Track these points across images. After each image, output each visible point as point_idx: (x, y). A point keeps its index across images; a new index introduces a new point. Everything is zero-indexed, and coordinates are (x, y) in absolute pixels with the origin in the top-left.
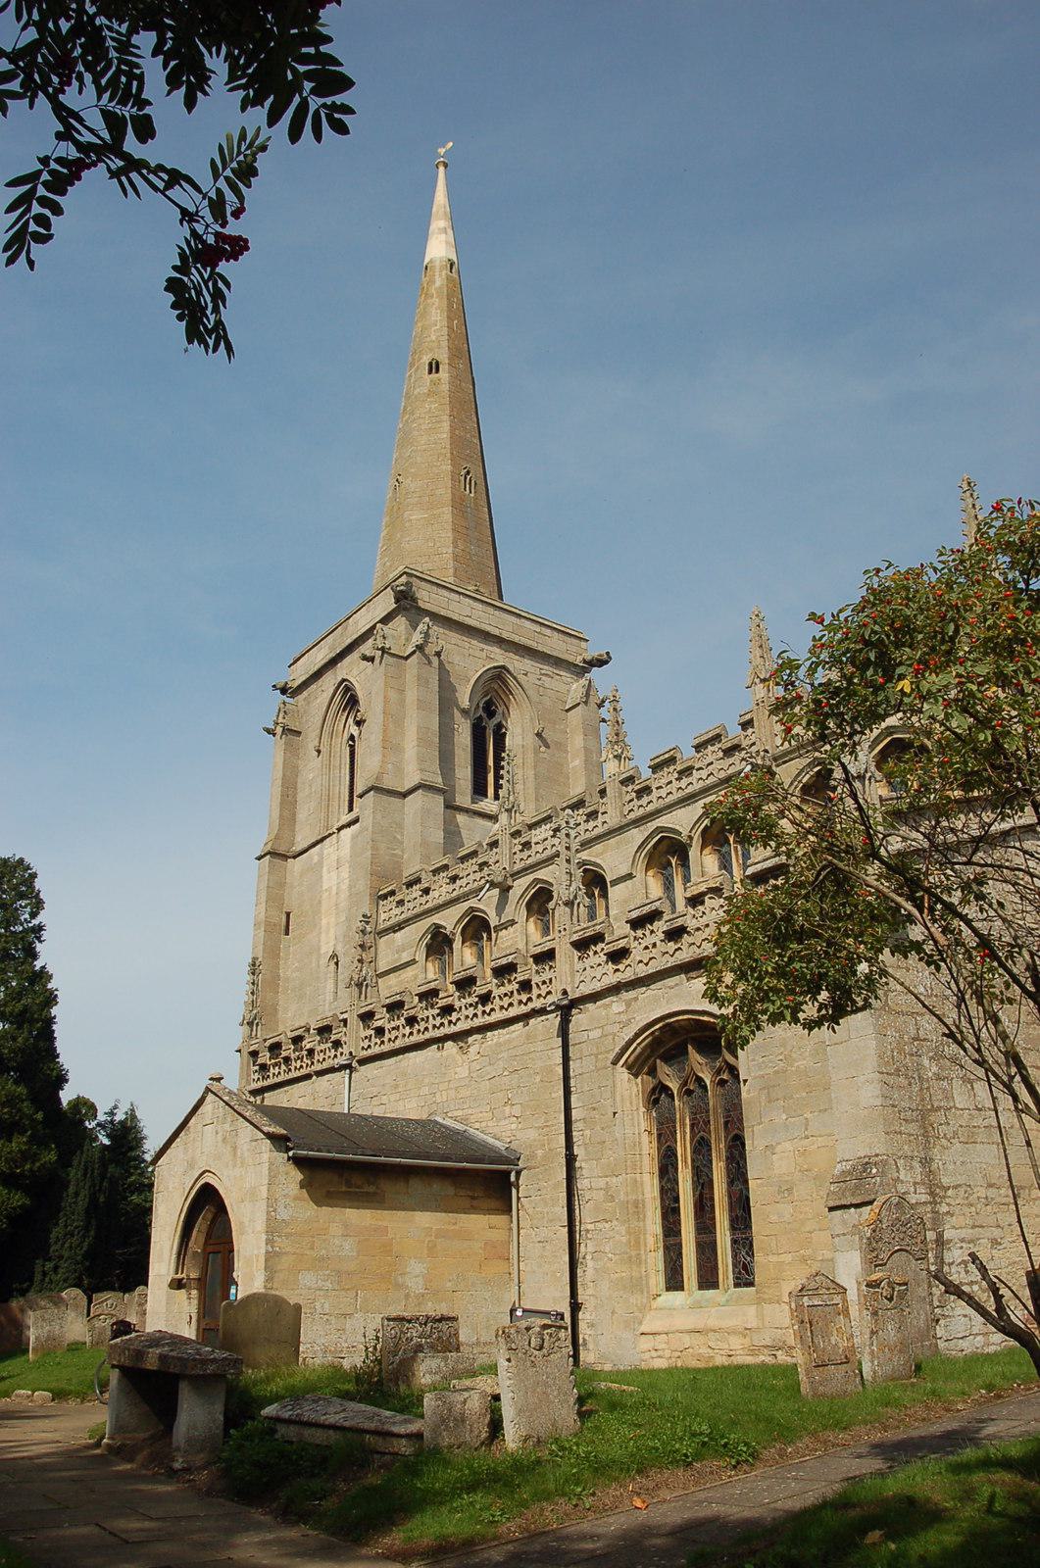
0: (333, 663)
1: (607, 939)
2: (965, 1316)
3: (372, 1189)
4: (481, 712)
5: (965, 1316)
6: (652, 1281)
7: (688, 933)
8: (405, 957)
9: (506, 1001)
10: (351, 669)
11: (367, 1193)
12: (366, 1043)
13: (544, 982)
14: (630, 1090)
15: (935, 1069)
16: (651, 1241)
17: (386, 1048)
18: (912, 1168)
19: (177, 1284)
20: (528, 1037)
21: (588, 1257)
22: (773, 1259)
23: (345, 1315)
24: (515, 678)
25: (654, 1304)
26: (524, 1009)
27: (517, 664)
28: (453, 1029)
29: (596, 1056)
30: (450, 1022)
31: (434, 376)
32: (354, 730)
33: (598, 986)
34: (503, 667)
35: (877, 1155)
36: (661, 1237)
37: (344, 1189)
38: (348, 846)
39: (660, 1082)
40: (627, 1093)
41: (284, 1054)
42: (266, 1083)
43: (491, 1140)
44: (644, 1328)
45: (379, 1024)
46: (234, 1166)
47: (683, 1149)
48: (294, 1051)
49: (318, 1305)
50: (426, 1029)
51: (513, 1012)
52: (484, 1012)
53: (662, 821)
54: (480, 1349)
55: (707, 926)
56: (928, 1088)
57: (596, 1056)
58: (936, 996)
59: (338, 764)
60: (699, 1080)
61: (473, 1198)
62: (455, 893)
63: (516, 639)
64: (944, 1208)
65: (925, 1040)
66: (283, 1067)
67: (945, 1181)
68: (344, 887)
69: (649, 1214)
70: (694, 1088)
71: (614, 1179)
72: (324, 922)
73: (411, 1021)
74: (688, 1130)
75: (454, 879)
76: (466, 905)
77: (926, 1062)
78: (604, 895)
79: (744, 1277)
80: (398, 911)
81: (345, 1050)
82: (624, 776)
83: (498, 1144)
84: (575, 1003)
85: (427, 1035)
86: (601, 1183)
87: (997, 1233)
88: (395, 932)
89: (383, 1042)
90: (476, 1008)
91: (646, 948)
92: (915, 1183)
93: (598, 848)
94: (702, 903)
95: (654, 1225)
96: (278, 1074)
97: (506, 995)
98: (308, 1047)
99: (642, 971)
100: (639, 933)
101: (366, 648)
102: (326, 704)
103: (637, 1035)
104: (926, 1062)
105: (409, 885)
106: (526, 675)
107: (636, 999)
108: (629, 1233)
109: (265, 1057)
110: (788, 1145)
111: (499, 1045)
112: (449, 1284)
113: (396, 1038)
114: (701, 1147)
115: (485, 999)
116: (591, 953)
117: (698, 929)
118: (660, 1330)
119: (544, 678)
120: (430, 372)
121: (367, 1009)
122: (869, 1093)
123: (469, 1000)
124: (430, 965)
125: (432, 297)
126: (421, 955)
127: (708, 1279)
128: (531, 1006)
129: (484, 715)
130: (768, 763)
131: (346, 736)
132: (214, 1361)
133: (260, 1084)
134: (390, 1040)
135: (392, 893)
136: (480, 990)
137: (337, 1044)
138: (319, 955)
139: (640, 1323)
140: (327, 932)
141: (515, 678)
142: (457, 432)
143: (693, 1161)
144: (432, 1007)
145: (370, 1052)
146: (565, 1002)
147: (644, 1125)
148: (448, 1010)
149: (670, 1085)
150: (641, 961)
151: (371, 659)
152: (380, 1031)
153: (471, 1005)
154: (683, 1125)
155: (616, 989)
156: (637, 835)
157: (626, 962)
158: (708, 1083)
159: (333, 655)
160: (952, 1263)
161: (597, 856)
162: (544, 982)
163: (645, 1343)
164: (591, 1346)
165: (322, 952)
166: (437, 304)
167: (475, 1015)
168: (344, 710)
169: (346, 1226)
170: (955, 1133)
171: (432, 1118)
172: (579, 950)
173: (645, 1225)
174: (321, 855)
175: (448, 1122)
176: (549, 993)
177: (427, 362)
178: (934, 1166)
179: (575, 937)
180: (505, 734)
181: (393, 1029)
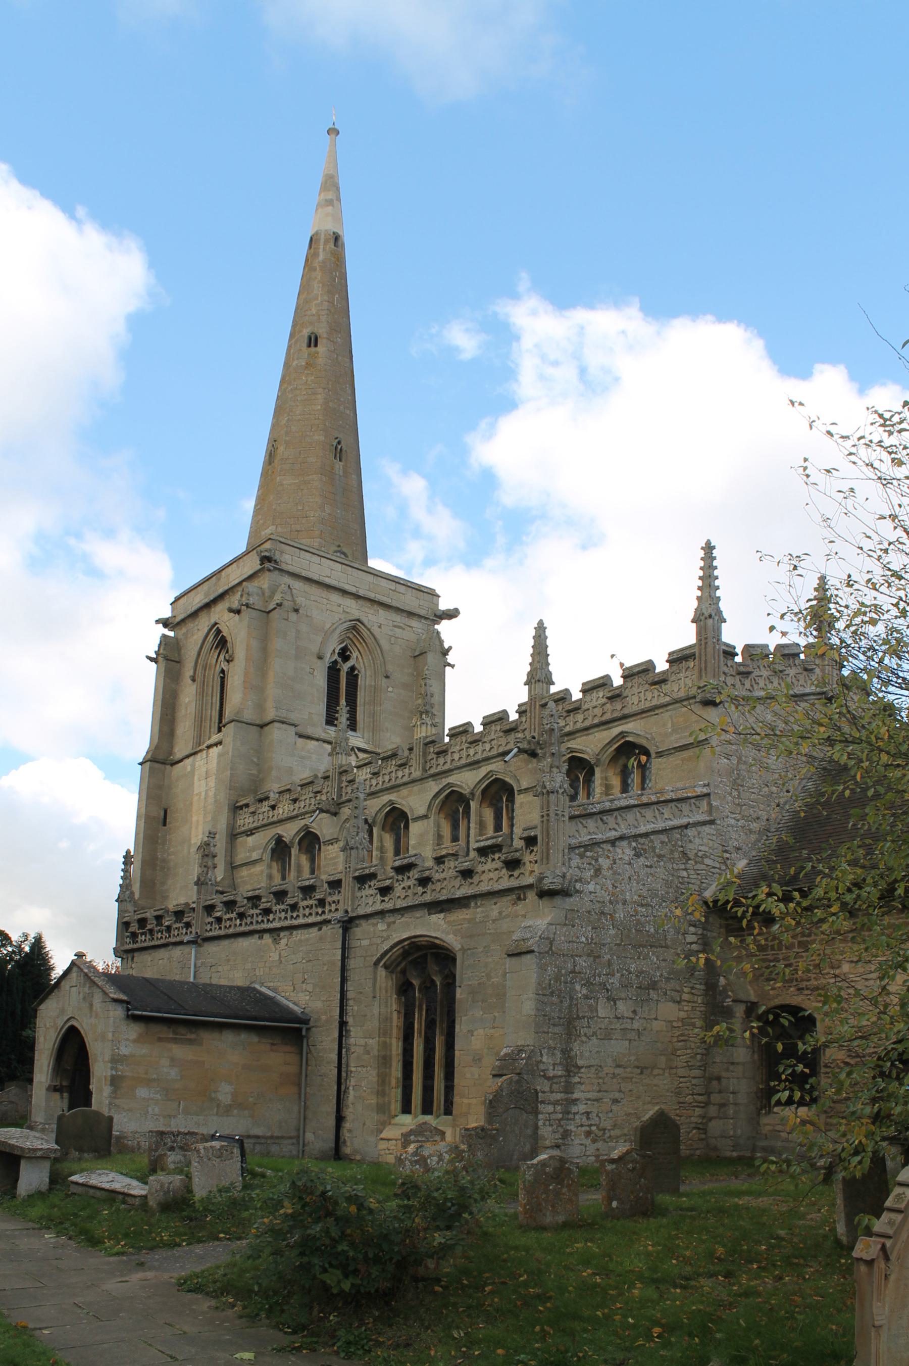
0: (208, 606)
1: (379, 878)
2: (582, 1145)
3: (193, 1036)
4: (336, 657)
5: (582, 1145)
6: (393, 1107)
7: (433, 883)
8: (255, 856)
9: (307, 911)
10: (220, 615)
11: (190, 1040)
12: (209, 927)
13: (334, 902)
14: (384, 980)
15: (584, 991)
16: (393, 1082)
17: (222, 932)
18: (553, 1054)
19: (54, 1089)
20: (321, 938)
21: (351, 1088)
22: (465, 1101)
23: (170, 1116)
24: (369, 630)
25: (393, 1121)
26: (319, 919)
27: (374, 618)
28: (270, 926)
29: (365, 957)
30: (268, 920)
31: (313, 349)
32: (224, 665)
33: (369, 910)
34: (358, 620)
35: (528, 1046)
36: (401, 1080)
37: (171, 1036)
38: (215, 761)
39: (408, 980)
40: (384, 985)
41: (149, 927)
42: (135, 946)
43: (291, 1005)
44: (383, 1135)
45: (218, 914)
46: (91, 1017)
47: (419, 1025)
48: (157, 925)
49: (150, 1109)
50: (252, 923)
51: (310, 920)
52: (292, 917)
53: (452, 779)
54: (272, 1141)
55: (445, 879)
56: (576, 1005)
57: (365, 957)
58: (595, 944)
59: (210, 692)
60: (433, 982)
61: (273, 1044)
62: (295, 812)
63: (372, 595)
64: (577, 1079)
65: (580, 973)
66: (148, 936)
67: (580, 1063)
68: (211, 794)
69: (394, 1064)
70: (428, 986)
71: (371, 1041)
72: (194, 819)
73: (241, 916)
74: (424, 1013)
75: (295, 801)
76: (303, 823)
77: (578, 987)
78: (407, 827)
79: (448, 1111)
80: (251, 819)
81: (193, 930)
82: (428, 740)
83: (296, 1008)
84: (352, 920)
85: (251, 928)
86: (362, 1042)
87: (617, 1095)
88: (248, 836)
89: (220, 928)
90: (286, 913)
91: (404, 888)
92: (554, 1065)
93: (404, 791)
94: (443, 863)
95: (396, 1071)
96: (144, 940)
97: (307, 907)
98: (167, 924)
99: (400, 904)
100: (400, 877)
101: (234, 601)
102: (200, 642)
103: (392, 947)
104: (578, 987)
105: (261, 801)
106: (380, 627)
107: (394, 922)
108: (378, 1075)
109: (134, 927)
110: (481, 1031)
111: (300, 941)
112: (251, 1099)
113: (230, 926)
114: (431, 1025)
115: (294, 907)
116: (367, 886)
117: (439, 881)
118: (392, 1137)
119: (396, 629)
120: (309, 346)
121: (210, 903)
122: (528, 1006)
123: (282, 907)
124: (274, 864)
125: (315, 270)
126: (267, 856)
127: (427, 1109)
128: (324, 917)
129: (339, 660)
130: (533, 747)
131: (218, 669)
132: (41, 1149)
133: (131, 946)
134: (226, 927)
135: (247, 806)
136: (290, 901)
137: (188, 925)
138: (190, 845)
139: (381, 1132)
140: (197, 828)
141: (369, 630)
142: (331, 404)
143: (425, 1033)
144: (256, 908)
145: (211, 934)
146: (346, 918)
147: (394, 1007)
148: (267, 912)
149: (414, 982)
150: (399, 897)
151: (238, 612)
152: (219, 920)
153: (283, 910)
154: (420, 1009)
155: (381, 913)
156: (433, 787)
157: (389, 896)
158: (438, 983)
159: (207, 600)
160: (577, 1113)
161: (403, 798)
162: (334, 902)
163: (383, 1145)
164: (348, 1144)
165: (193, 842)
166: (319, 277)
167: (286, 918)
168: (216, 648)
169: (172, 1060)
170: (594, 1034)
171: (253, 985)
172: (358, 883)
173: (390, 1071)
174: (193, 766)
175: (263, 990)
176: (337, 910)
177: (306, 335)
178: (573, 1053)
179: (357, 874)
180: (357, 675)
181: (228, 919)
